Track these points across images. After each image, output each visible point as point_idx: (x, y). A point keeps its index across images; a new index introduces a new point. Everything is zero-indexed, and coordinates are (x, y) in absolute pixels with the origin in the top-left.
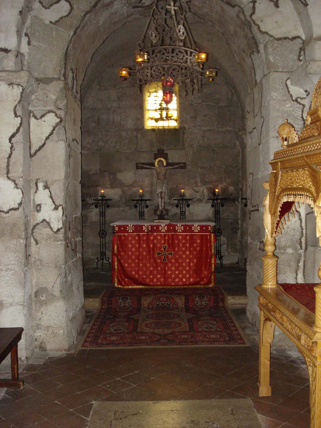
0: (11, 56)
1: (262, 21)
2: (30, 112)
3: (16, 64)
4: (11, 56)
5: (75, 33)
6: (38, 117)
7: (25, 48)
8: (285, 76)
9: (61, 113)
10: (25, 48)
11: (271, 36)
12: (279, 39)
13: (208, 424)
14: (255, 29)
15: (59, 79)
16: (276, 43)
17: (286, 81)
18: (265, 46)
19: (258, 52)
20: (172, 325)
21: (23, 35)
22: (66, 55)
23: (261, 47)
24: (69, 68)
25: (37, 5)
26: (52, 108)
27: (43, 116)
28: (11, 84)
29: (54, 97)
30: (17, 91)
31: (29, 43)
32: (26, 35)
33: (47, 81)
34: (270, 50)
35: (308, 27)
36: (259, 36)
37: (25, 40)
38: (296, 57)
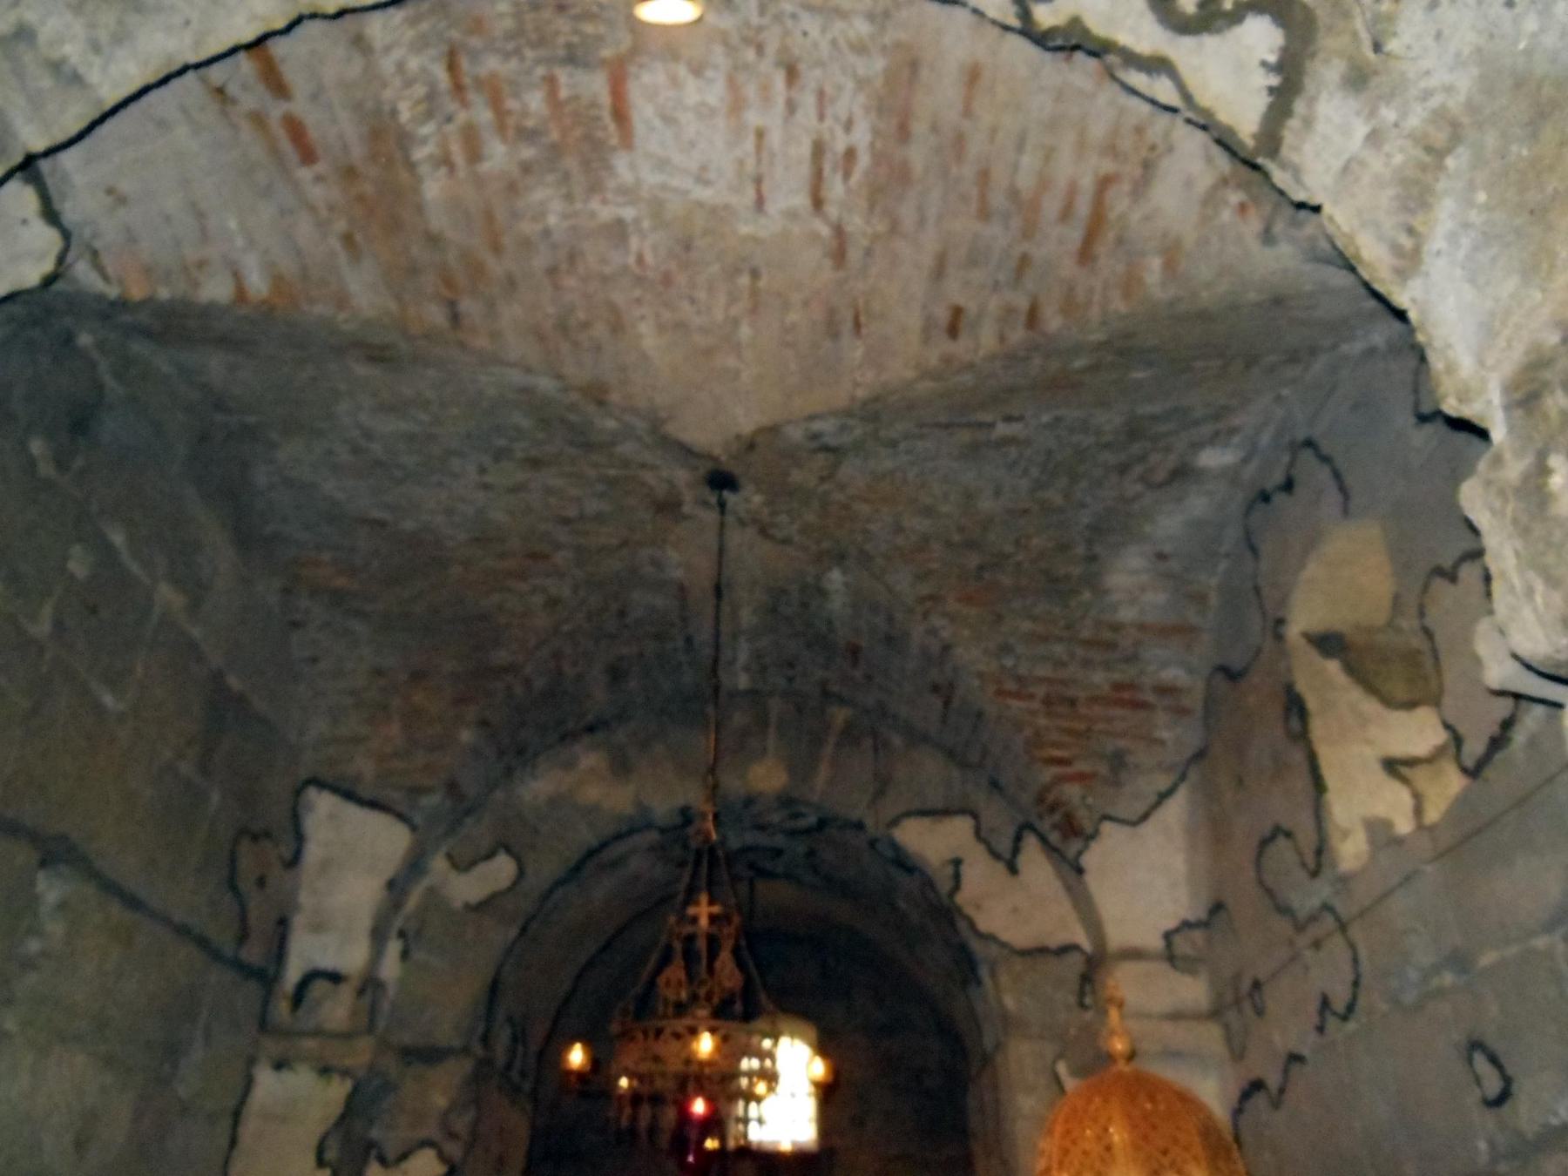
0: (346, 993)
1: (978, 907)
2: (371, 1145)
3: (354, 1013)
4: (346, 993)
5: (524, 930)
6: (391, 1155)
7: (390, 968)
8: (1049, 1050)
9: (454, 1150)
10: (390, 968)
11: (1004, 945)
12: (1025, 953)
13: (590, 717)
14: (962, 925)
15: (466, 1050)
16: (1018, 965)
17: (1054, 1062)
18: (993, 974)
19: (979, 982)
20: (540, 215)
21: (394, 933)
22: (494, 989)
23: (984, 972)
24: (500, 1015)
25: (439, 864)
26: (431, 1130)
27: (404, 1157)
28: (325, 1071)
29: (440, 1101)
30: (338, 1090)
31: (405, 955)
32: (402, 934)
33: (426, 1055)
34: (1004, 979)
35: (1093, 924)
36: (976, 946)
37: (394, 947)
38: (1072, 999)
